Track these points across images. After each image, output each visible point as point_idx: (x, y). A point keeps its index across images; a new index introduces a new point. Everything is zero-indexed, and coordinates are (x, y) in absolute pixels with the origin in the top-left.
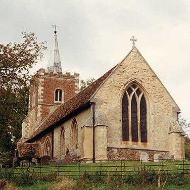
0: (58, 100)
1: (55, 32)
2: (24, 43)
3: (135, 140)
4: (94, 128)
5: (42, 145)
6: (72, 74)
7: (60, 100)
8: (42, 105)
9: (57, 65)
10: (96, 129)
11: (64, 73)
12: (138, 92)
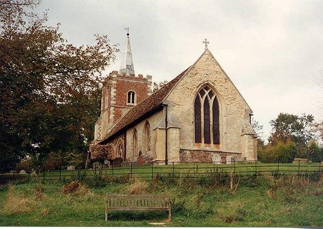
1: (128, 35)
3: (207, 142)
4: (167, 130)
5: (114, 147)
7: (133, 102)
9: (130, 67)
11: (137, 76)
12: (211, 94)
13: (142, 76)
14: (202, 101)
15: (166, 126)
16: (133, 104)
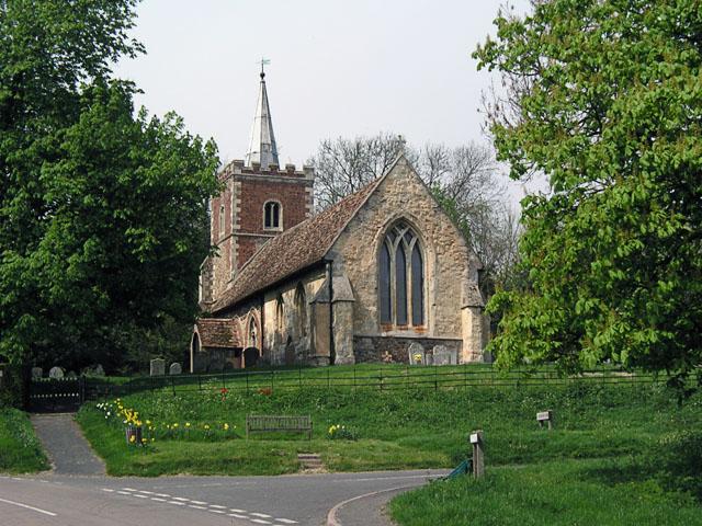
0: (272, 224)
1: (263, 75)
2: (508, 87)
3: (402, 323)
4: (331, 304)
5: (242, 323)
6: (299, 169)
7: (276, 225)
8: (240, 236)
9: (270, 147)
10: (334, 306)
11: (282, 168)
12: (409, 235)
13: (293, 168)
14: (393, 250)
15: (331, 298)
16: (274, 229)
